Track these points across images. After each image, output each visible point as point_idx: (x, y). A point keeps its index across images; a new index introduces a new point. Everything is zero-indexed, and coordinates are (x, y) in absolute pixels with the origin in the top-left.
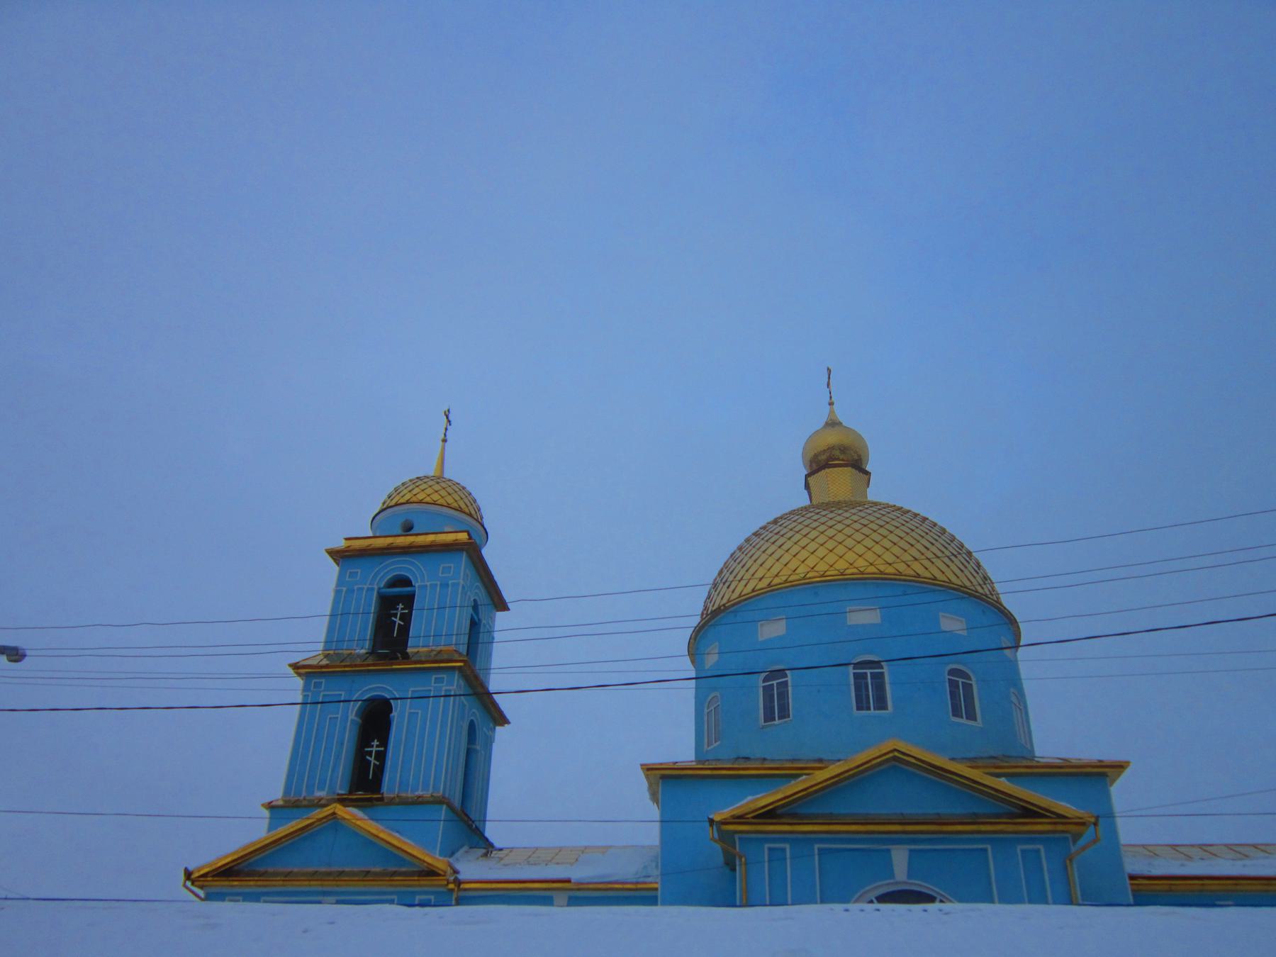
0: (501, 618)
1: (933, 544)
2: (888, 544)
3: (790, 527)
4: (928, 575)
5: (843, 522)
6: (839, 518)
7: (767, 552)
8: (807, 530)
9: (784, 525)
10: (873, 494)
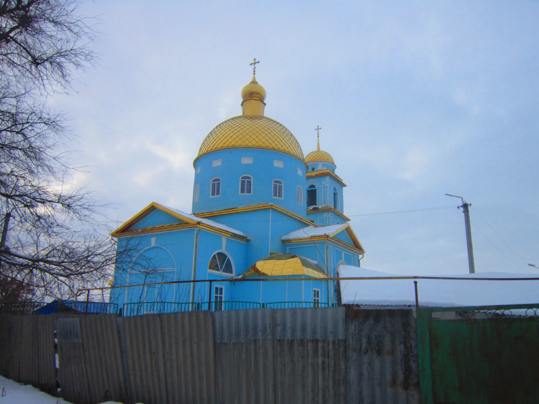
0: (248, 238)
4: (288, 151)
7: (233, 132)
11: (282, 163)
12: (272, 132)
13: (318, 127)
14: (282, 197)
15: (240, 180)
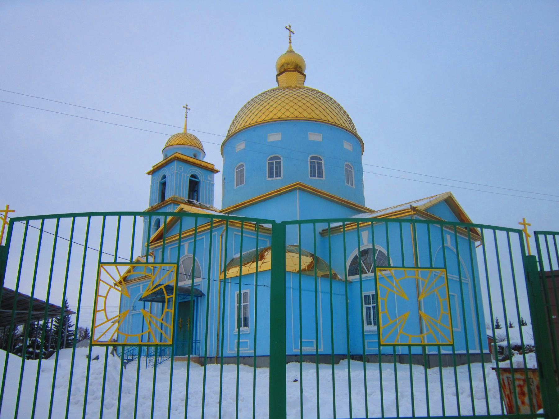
1: (331, 105)
2: (314, 109)
3: (266, 97)
5: (293, 96)
6: (287, 93)
8: (273, 98)
9: (261, 104)
10: (306, 85)
11: (320, 135)
12: (316, 103)
13: (184, 107)
14: (322, 177)
15: (268, 162)
